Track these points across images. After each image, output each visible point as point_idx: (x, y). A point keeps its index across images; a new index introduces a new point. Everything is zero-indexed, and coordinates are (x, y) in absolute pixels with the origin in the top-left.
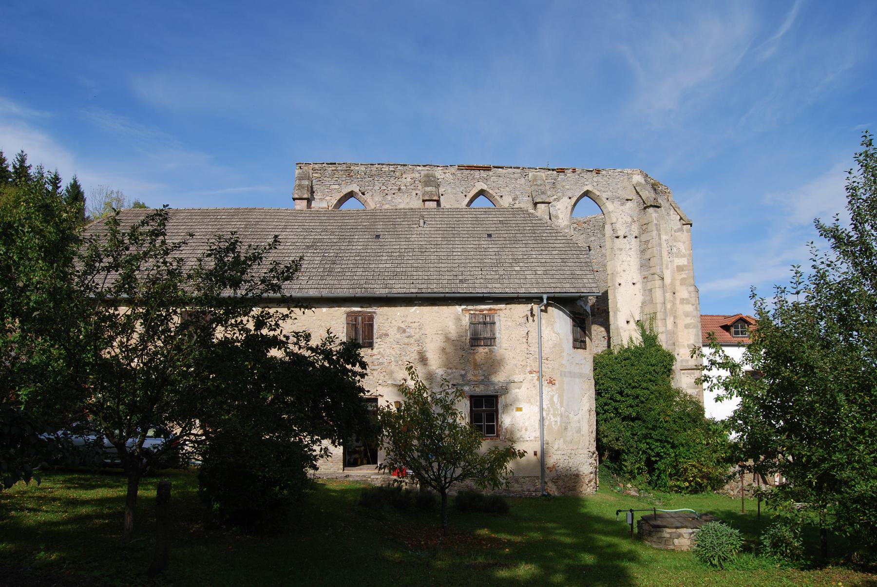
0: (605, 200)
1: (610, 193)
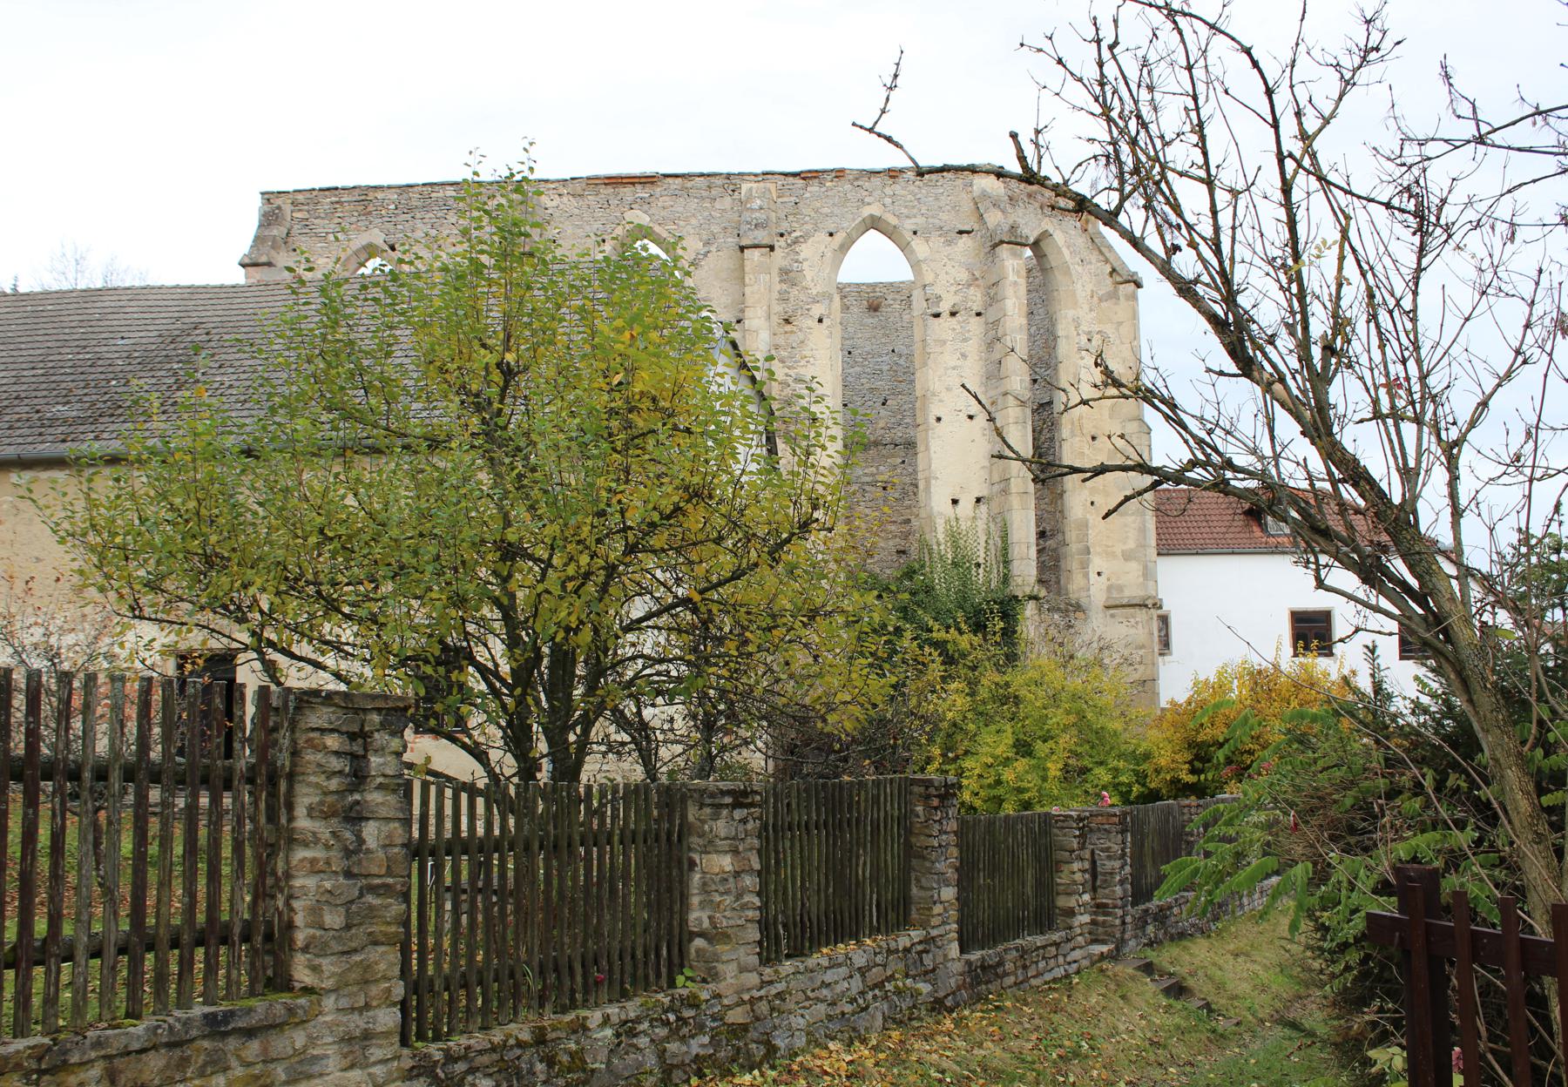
1: (920, 220)
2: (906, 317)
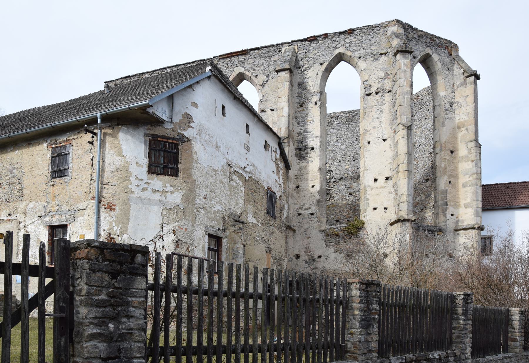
0: (356, 59)
1: (362, 51)
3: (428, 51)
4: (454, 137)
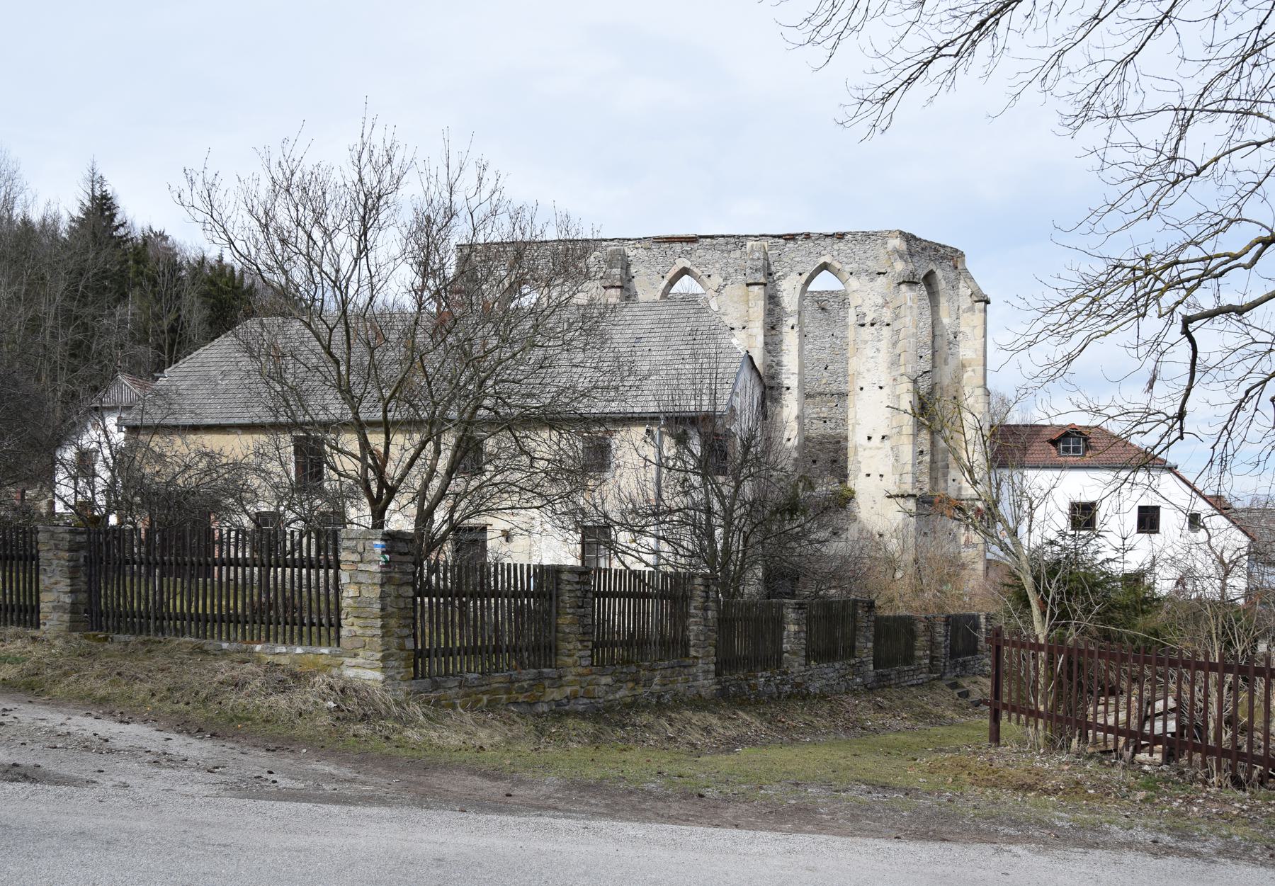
1: (854, 265)
2: (841, 313)
3: (932, 266)
4: (958, 380)
